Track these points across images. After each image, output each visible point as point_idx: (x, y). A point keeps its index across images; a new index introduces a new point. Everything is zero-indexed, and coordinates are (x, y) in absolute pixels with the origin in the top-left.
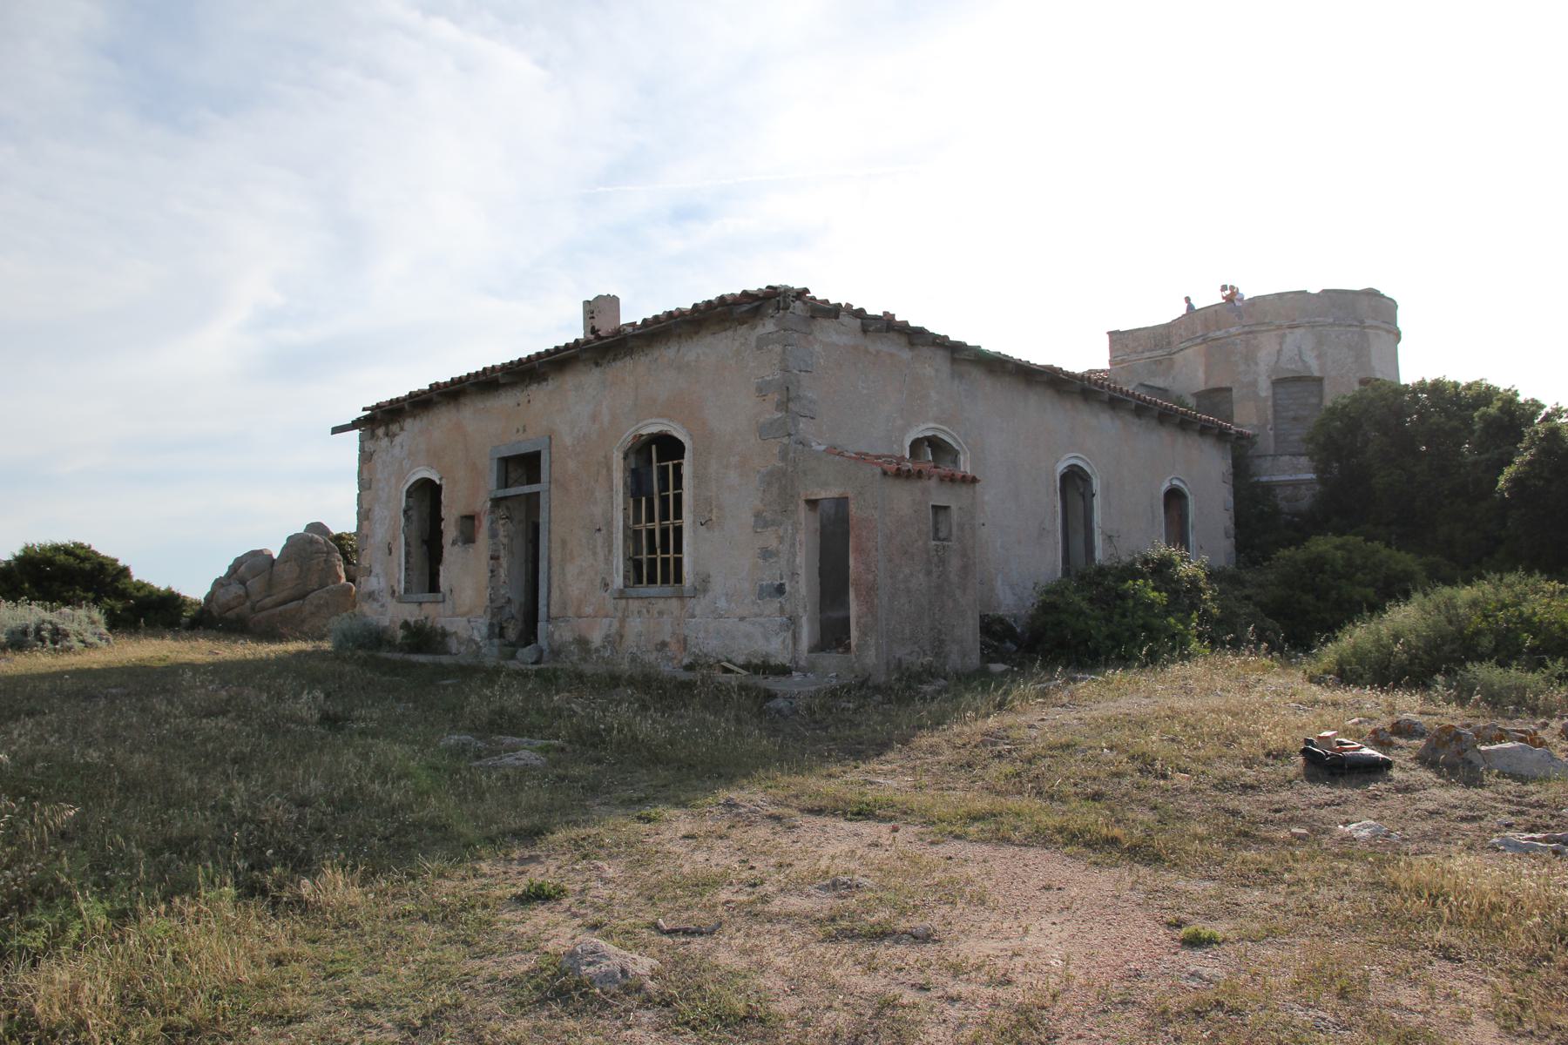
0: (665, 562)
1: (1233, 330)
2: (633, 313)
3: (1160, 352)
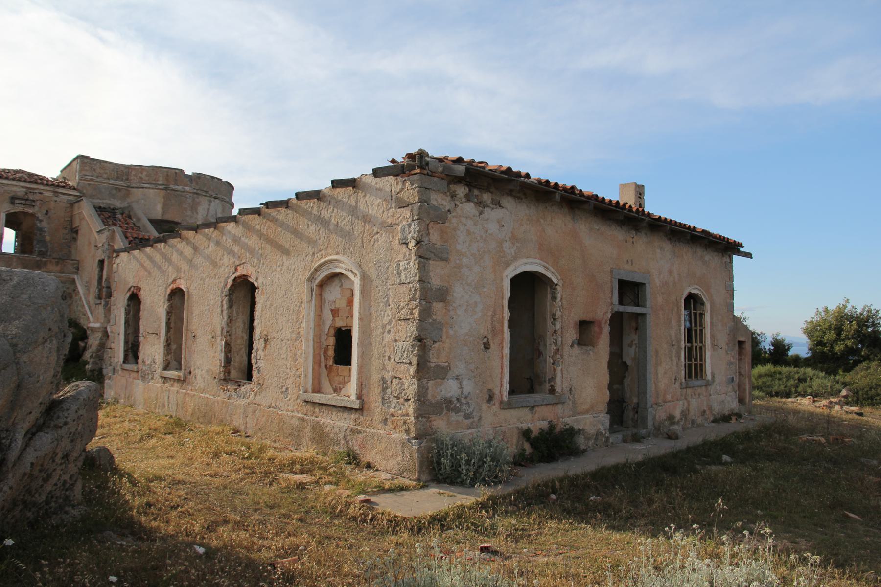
0: (696, 365)
1: (187, 189)
2: (654, 207)
3: (120, 183)
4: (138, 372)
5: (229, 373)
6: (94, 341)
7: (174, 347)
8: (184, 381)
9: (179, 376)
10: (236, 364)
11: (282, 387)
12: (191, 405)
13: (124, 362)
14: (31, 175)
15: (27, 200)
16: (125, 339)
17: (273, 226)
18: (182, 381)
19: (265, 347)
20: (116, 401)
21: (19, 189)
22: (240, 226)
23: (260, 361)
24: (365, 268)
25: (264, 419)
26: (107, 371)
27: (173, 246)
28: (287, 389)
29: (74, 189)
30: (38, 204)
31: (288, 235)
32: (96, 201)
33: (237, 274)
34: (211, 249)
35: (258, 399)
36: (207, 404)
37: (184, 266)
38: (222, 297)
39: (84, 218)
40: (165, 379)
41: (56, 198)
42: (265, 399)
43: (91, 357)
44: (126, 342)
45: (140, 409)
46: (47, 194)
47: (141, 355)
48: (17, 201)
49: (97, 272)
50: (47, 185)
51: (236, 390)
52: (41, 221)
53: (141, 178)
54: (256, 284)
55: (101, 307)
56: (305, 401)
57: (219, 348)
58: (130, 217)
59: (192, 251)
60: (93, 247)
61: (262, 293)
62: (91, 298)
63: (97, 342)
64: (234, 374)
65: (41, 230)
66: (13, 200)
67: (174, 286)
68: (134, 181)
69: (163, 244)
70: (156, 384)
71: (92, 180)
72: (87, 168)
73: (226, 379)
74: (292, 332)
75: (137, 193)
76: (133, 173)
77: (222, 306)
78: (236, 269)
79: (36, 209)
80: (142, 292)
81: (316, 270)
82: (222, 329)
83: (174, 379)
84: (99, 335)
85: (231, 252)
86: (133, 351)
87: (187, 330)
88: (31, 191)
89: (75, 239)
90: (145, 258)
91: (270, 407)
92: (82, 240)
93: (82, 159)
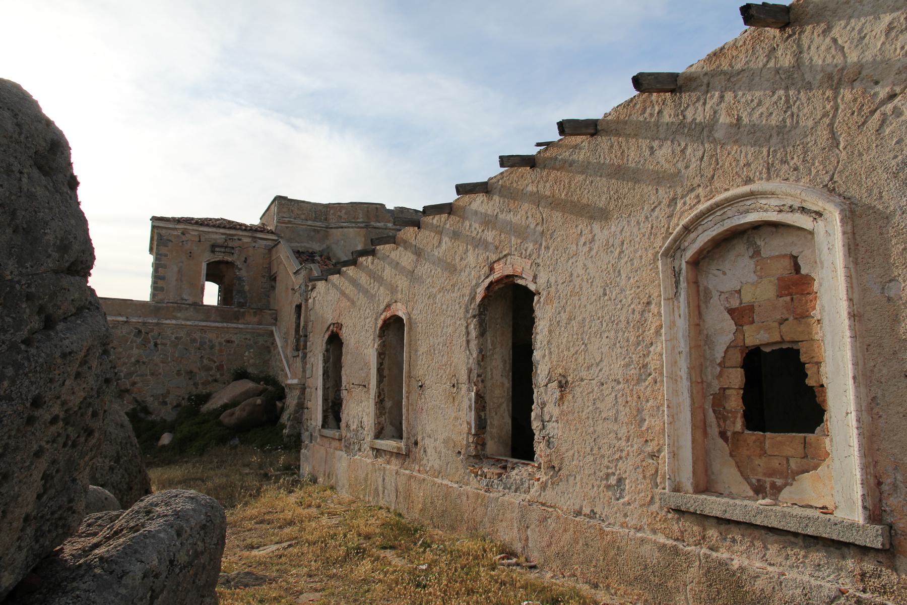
4: (340, 440)
5: (483, 445)
6: (291, 401)
7: (388, 404)
8: (407, 455)
9: (399, 448)
10: (494, 431)
11: (608, 476)
12: (420, 495)
13: (323, 426)
14: (230, 222)
15: (227, 248)
16: (323, 395)
17: (564, 176)
18: (405, 456)
19: (562, 398)
20: (314, 481)
21: (218, 236)
22: (496, 198)
23: (550, 426)
24: (854, 191)
25: (567, 536)
26: (305, 436)
27: (385, 258)
28: (620, 481)
29: (272, 233)
30: (237, 251)
31: (602, 182)
32: (293, 245)
33: (496, 276)
34: (444, 246)
35: (549, 496)
36: (446, 497)
37: (402, 283)
38: (466, 319)
39: (281, 262)
40: (378, 452)
41: (254, 244)
42: (567, 498)
43: (289, 419)
44: (325, 400)
45: (345, 495)
46: (246, 240)
47: (344, 417)
48: (217, 249)
49: (294, 320)
50: (245, 230)
51: (500, 475)
52: (240, 269)
53: (340, 217)
54: (532, 287)
55: (299, 360)
56: (677, 511)
57: (466, 403)
58: (329, 259)
59: (413, 257)
60: (290, 292)
61: (549, 300)
62: (290, 351)
63: (295, 402)
64: (491, 447)
65: (240, 279)
66: (213, 248)
67: (388, 314)
68: (333, 220)
69: (370, 258)
70: (365, 459)
71: (289, 222)
72: (285, 210)
73: (478, 455)
74: (627, 365)
75: (336, 234)
76: (332, 212)
77: (468, 333)
78: (492, 269)
79: (236, 256)
80: (344, 329)
81: (687, 229)
82: (470, 371)
83: (392, 453)
84: (297, 393)
85: (480, 244)
86: (333, 411)
87: (410, 377)
88: (230, 237)
89: (273, 288)
90: (347, 283)
91: (578, 513)
92: (280, 286)
93: (281, 202)
